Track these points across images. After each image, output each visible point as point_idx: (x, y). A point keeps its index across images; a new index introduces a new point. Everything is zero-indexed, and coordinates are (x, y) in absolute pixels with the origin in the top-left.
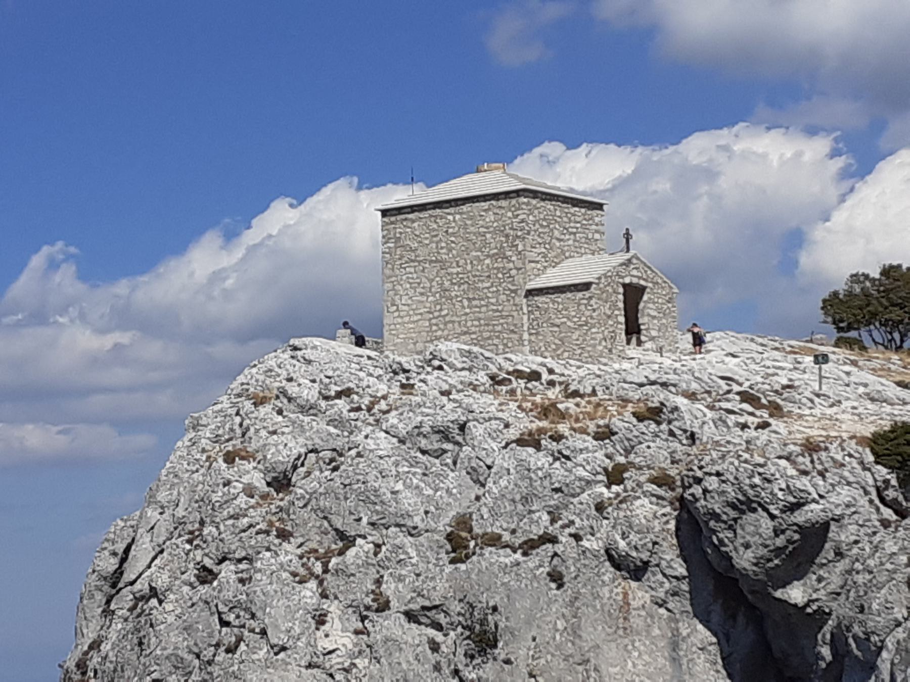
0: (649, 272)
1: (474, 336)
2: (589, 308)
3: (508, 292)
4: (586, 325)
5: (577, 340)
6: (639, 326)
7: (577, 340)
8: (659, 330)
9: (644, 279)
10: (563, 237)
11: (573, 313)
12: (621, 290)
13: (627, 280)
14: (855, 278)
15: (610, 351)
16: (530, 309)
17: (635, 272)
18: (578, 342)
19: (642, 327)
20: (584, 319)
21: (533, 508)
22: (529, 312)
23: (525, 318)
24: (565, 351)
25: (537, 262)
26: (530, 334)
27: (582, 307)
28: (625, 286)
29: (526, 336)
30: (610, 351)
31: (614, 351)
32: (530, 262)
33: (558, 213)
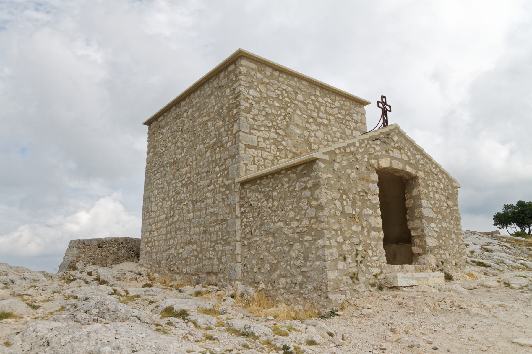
0: (418, 157)
1: (195, 246)
2: (314, 203)
3: (222, 190)
4: (308, 234)
5: (297, 258)
6: (409, 231)
7: (297, 258)
8: (438, 239)
9: (410, 165)
10: (307, 125)
11: (292, 214)
12: (375, 177)
13: (385, 163)
14: (506, 207)
15: (354, 277)
16: (243, 210)
17: (396, 153)
18: (298, 263)
19: (413, 233)
20: (305, 222)
21: (362, 321)
22: (242, 213)
23: (238, 222)
24: (281, 276)
25: (263, 149)
26: (243, 246)
27: (304, 204)
28: (382, 172)
29: (238, 250)
30: (354, 277)
31: (362, 278)
32: (248, 146)
33: (300, 97)
